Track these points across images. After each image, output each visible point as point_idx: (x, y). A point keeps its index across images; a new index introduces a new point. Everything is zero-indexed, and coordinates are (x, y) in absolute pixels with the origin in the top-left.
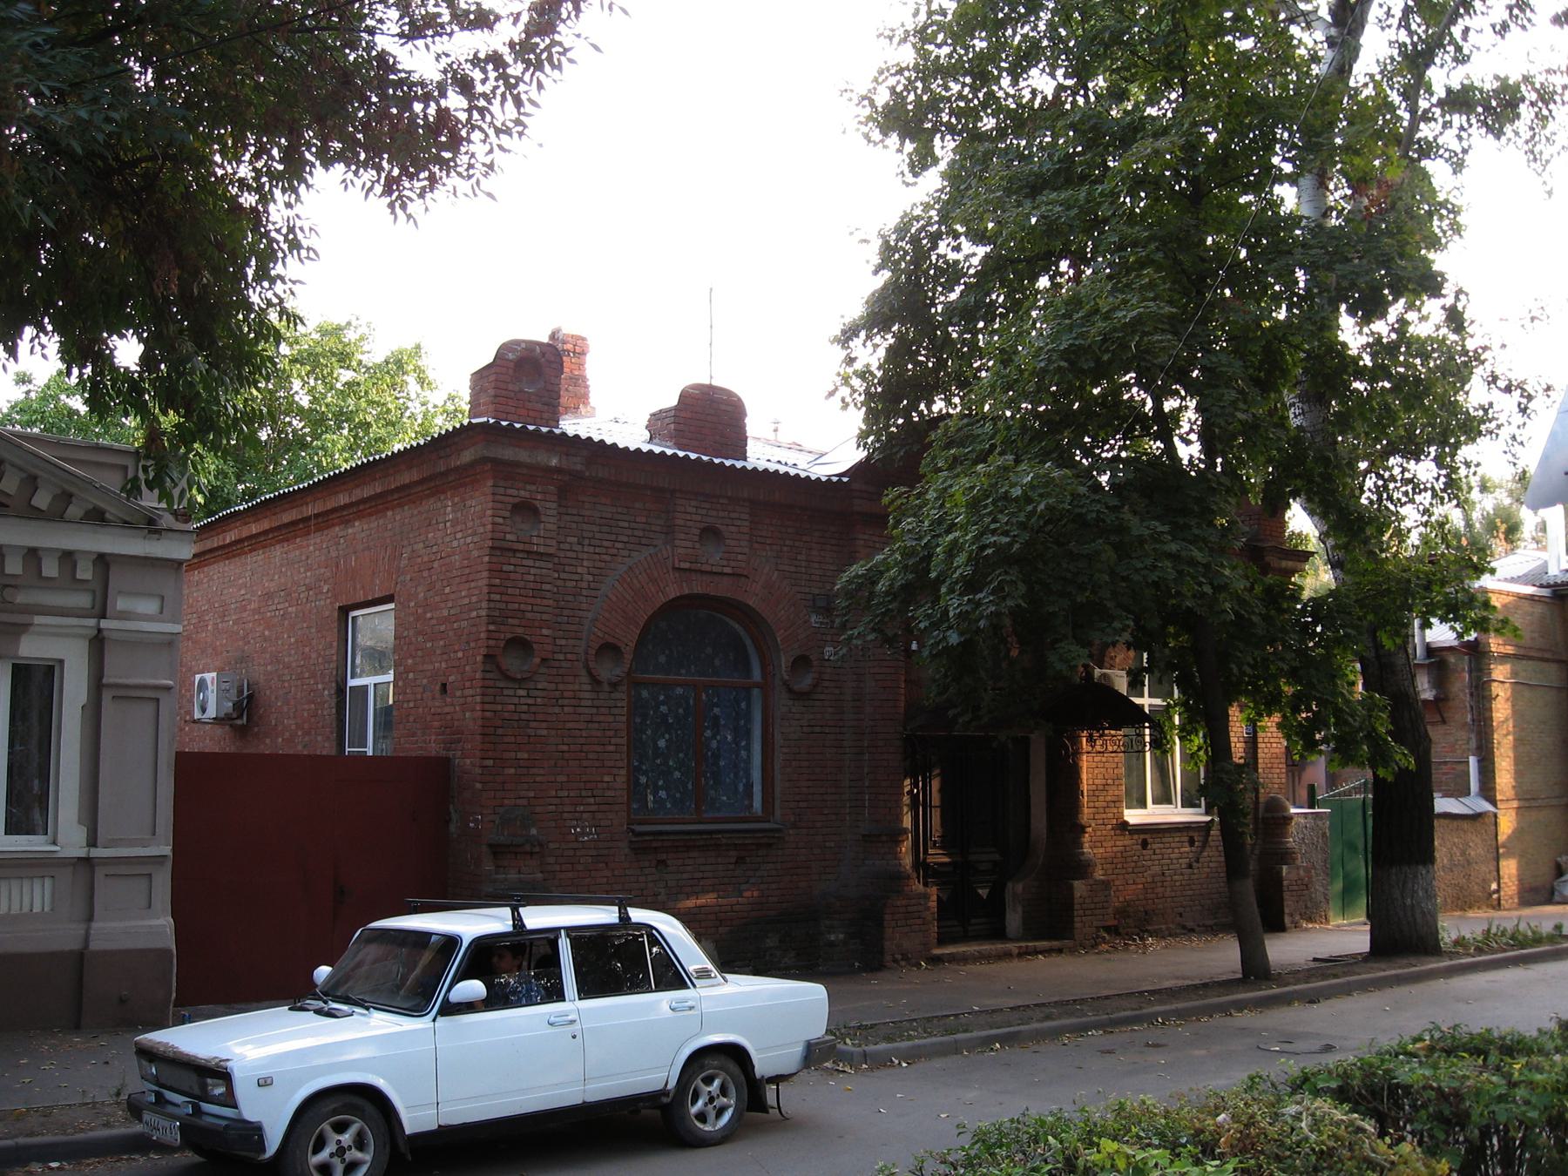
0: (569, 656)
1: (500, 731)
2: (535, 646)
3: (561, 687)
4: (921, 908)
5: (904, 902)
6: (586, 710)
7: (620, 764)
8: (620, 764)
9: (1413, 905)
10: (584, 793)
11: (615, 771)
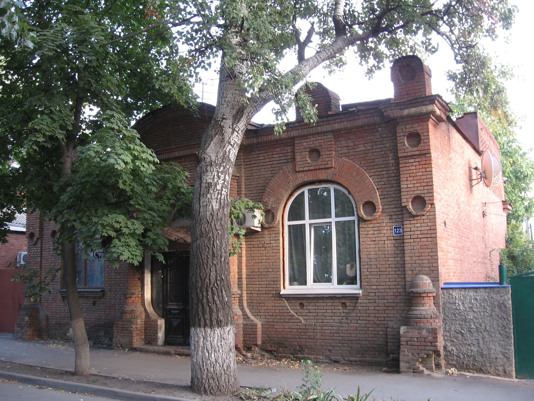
4: (128, 326)
5: (121, 323)
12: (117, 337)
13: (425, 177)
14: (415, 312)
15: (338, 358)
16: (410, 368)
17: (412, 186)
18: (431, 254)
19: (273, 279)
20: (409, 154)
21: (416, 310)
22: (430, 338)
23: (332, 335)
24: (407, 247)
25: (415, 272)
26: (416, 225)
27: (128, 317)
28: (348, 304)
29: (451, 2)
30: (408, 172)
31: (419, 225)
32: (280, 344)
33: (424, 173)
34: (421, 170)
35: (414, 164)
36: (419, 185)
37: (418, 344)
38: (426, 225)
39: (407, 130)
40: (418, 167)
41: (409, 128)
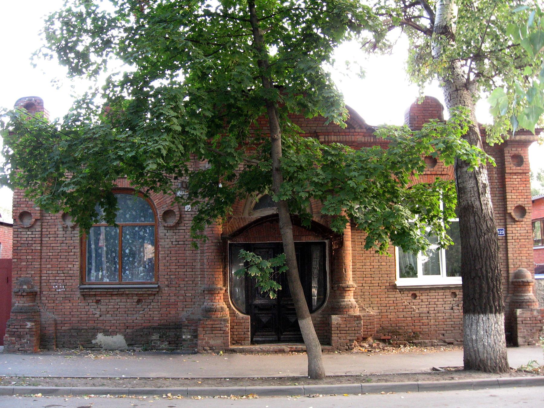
0: (53, 217)
1: (19, 248)
2: (32, 214)
3: (49, 230)
4: (221, 326)
5: (211, 323)
6: (61, 239)
7: (76, 260)
8: (76, 260)
9: (476, 340)
10: (59, 272)
11: (74, 263)
12: (203, 339)
13: (525, 191)
14: (525, 298)
15: (451, 340)
16: (525, 342)
17: (515, 197)
18: (528, 252)
19: (387, 272)
20: (514, 171)
21: (526, 296)
22: (540, 317)
23: (444, 320)
24: (510, 246)
25: (516, 266)
26: (517, 229)
27: (219, 316)
28: (457, 293)
29: (162, 2)
30: (512, 186)
31: (519, 229)
32: (394, 332)
33: (525, 188)
34: (522, 185)
35: (517, 180)
36: (521, 197)
37: (531, 322)
38: (524, 229)
39: (513, 152)
40: (520, 183)
41: (514, 151)
